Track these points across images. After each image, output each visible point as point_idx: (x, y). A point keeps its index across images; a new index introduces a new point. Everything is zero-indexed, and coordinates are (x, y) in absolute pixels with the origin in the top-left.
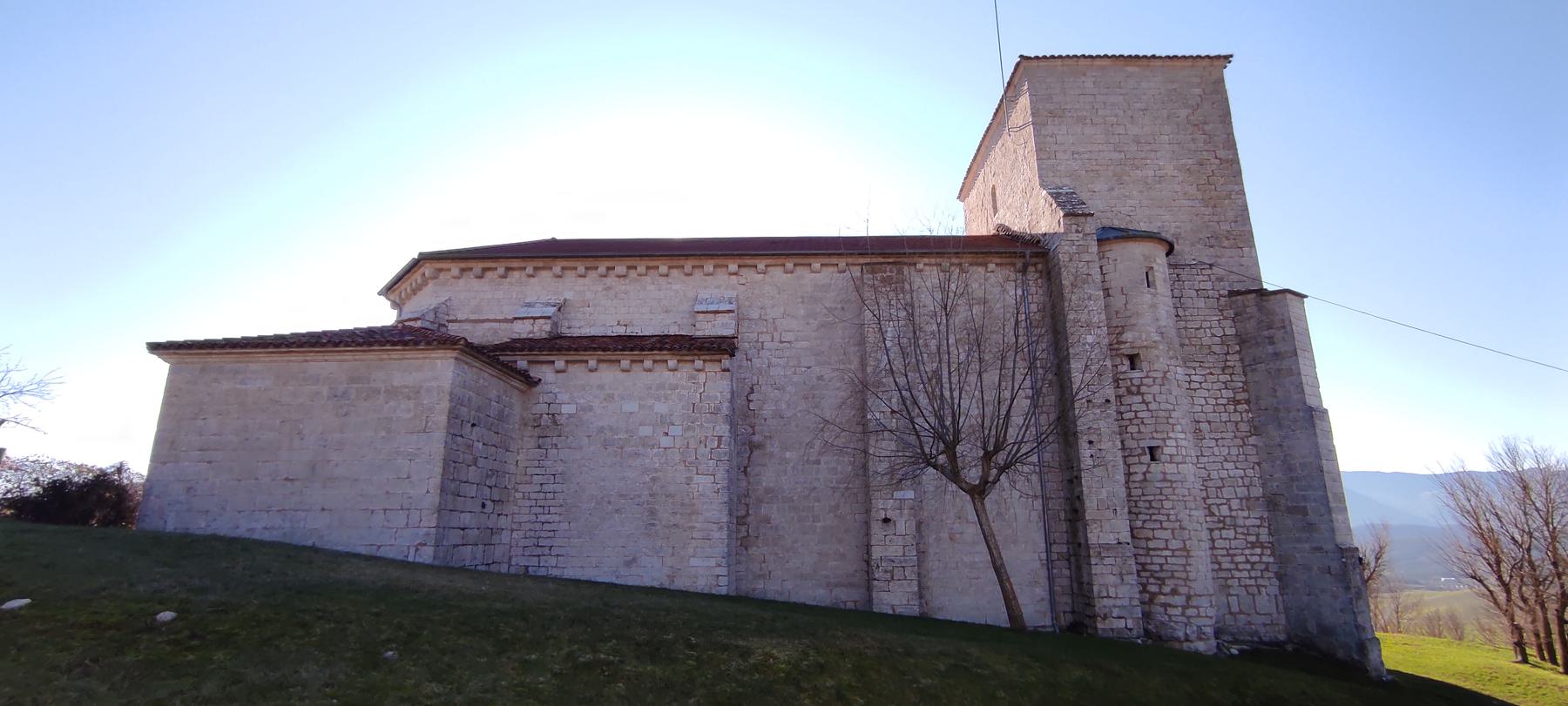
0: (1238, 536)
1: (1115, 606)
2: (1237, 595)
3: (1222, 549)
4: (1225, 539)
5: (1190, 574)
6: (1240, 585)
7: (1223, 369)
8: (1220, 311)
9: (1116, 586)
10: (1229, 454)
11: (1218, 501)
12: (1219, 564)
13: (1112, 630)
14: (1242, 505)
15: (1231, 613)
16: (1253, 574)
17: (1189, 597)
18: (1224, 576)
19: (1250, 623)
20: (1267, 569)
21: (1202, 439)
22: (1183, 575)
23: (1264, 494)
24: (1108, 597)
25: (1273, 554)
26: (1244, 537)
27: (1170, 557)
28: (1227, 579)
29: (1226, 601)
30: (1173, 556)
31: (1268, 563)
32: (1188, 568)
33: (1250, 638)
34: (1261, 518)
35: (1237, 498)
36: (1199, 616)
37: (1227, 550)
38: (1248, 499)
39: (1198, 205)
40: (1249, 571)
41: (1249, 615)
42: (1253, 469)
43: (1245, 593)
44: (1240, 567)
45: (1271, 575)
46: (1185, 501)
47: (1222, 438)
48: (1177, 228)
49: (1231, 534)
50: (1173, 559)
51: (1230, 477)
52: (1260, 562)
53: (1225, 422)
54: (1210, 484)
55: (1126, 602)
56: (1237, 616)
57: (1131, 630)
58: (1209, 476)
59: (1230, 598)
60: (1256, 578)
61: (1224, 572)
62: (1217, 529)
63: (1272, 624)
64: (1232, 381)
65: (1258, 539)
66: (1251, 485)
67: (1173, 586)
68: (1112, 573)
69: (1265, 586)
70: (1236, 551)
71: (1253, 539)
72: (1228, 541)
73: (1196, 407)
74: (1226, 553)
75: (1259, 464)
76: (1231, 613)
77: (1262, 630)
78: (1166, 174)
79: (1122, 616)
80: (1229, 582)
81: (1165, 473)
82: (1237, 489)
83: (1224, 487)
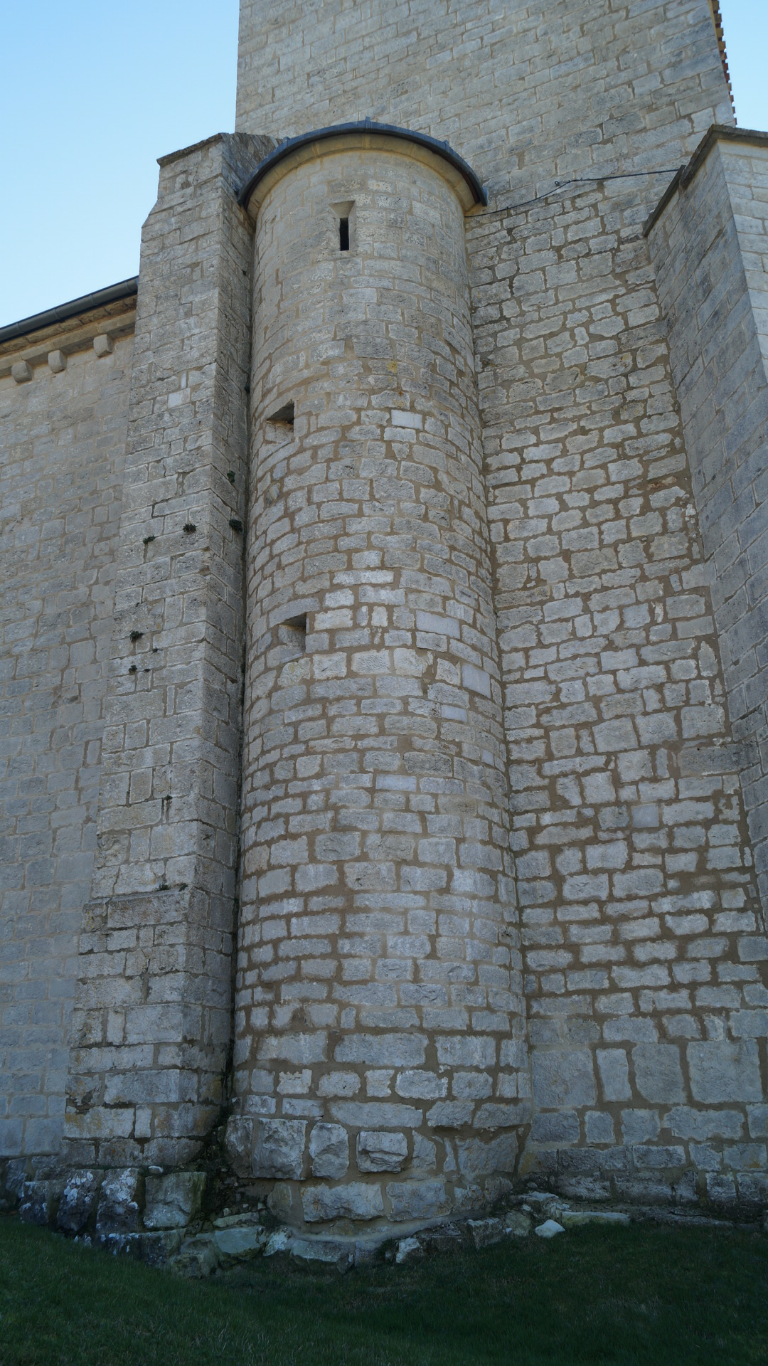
0: (638, 859)
1: (114, 1071)
2: (627, 1045)
3: (585, 903)
4: (596, 872)
5: (346, 963)
6: (638, 1013)
7: (616, 414)
8: (618, 276)
9: (125, 1010)
10: (620, 627)
11: (579, 764)
12: (574, 949)
13: (96, 1142)
14: (654, 768)
15: (603, 1105)
16: (683, 973)
17: (335, 1037)
18: (587, 985)
19: (666, 1137)
20: (731, 955)
21: (542, 603)
22: (327, 968)
23: (728, 724)
24: (105, 1044)
25: (752, 905)
26: (658, 860)
27: (297, 915)
28: (595, 994)
29: (590, 1066)
30: (305, 913)
31: (733, 937)
32: (345, 946)
33: (666, 1190)
34: (716, 796)
35: (641, 747)
36: (362, 1096)
37: (601, 904)
38: (674, 746)
39: (581, 66)
40: (669, 964)
41: (664, 1109)
42: (695, 656)
43: (655, 1035)
44: (641, 953)
45: (748, 973)
46: (362, 752)
47: (605, 589)
48: (523, 132)
49: (617, 853)
50: (306, 920)
51: (620, 691)
52: (708, 933)
53: (615, 546)
54: (558, 718)
55: (142, 1057)
56: (624, 1113)
57: (143, 1141)
58: (556, 695)
59: (601, 1054)
60: (693, 986)
61: (588, 973)
62: (572, 844)
63: (746, 1139)
64: (640, 435)
65: (702, 861)
66: (687, 703)
67: (297, 1005)
68: (122, 975)
69: (724, 1012)
70: (635, 904)
71: (685, 862)
72: (605, 877)
73: (533, 522)
74: (597, 915)
75: (712, 640)
76: (603, 1105)
77: (709, 1162)
78: (510, 31)
79: (126, 1100)
80: (603, 1004)
81: (309, 682)
82: (640, 721)
83: (601, 720)
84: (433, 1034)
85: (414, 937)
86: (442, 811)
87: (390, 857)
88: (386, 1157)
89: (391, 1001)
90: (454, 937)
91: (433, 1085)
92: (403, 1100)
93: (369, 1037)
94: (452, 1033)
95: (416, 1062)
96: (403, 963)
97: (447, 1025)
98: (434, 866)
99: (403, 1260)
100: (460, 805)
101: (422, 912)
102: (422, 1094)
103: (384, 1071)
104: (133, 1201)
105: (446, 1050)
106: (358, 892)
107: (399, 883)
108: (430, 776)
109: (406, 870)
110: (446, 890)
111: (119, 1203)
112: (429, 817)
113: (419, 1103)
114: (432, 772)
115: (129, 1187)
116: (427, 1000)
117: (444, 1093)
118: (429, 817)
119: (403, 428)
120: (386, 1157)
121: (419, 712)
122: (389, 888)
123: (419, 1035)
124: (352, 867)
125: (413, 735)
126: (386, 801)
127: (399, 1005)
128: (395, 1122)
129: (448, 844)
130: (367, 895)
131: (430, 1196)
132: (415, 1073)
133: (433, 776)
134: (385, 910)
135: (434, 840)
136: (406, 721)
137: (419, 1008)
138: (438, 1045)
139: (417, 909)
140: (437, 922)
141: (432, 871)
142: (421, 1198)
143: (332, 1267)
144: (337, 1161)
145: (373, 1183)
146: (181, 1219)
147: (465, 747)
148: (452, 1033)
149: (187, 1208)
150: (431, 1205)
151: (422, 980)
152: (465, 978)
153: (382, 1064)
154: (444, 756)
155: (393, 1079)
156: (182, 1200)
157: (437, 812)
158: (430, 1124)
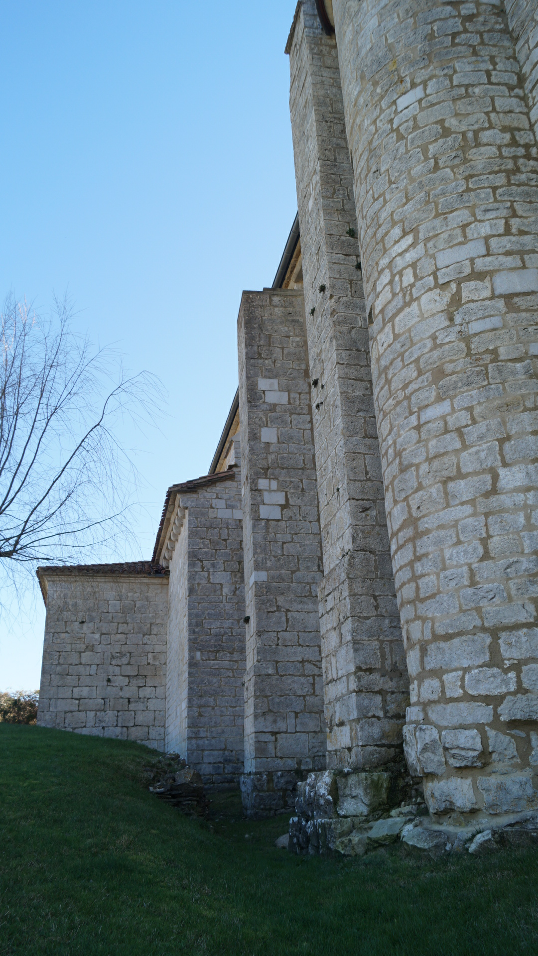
5: (420, 582)
36: (445, 700)
84: (495, 632)
85: (466, 545)
86: (478, 419)
87: (438, 479)
88: (463, 753)
89: (454, 608)
90: (508, 534)
91: (499, 680)
92: (473, 698)
93: (442, 645)
94: (517, 627)
95: (481, 661)
96: (460, 570)
97: (509, 620)
98: (476, 473)
99: (475, 851)
100: (499, 407)
101: (470, 520)
102: (488, 690)
103: (454, 673)
104: (329, 795)
105: (510, 645)
106: (419, 519)
107: (448, 500)
108: (464, 392)
109: (451, 485)
110: (494, 491)
111: (321, 796)
112: (465, 430)
113: (487, 699)
114: (465, 388)
115: (327, 784)
116: (486, 600)
117: (513, 687)
118: (465, 430)
119: (407, 108)
120: (463, 753)
121: (447, 340)
122: (441, 507)
123: (482, 635)
124: (414, 499)
125: (443, 364)
126: (429, 431)
127: (461, 610)
128: (470, 720)
129: (489, 449)
130: (426, 519)
131: (515, 789)
132: (480, 671)
133: (467, 391)
134: (441, 527)
135: (473, 450)
136: (436, 354)
137: (478, 610)
138: (500, 641)
139: (466, 517)
140: (486, 525)
141: (475, 478)
142: (507, 791)
143: (426, 853)
144: (436, 758)
145: (466, 778)
146: (364, 810)
147: (502, 351)
148: (517, 627)
149: (366, 801)
150: (519, 798)
151: (478, 583)
152: (526, 570)
153: (453, 667)
154: (476, 369)
155: (463, 679)
156: (362, 794)
157: (474, 422)
158: (502, 718)
